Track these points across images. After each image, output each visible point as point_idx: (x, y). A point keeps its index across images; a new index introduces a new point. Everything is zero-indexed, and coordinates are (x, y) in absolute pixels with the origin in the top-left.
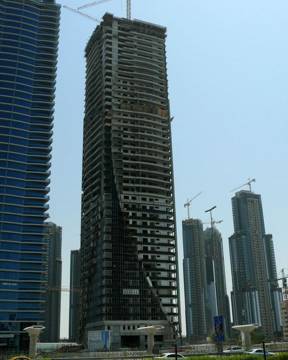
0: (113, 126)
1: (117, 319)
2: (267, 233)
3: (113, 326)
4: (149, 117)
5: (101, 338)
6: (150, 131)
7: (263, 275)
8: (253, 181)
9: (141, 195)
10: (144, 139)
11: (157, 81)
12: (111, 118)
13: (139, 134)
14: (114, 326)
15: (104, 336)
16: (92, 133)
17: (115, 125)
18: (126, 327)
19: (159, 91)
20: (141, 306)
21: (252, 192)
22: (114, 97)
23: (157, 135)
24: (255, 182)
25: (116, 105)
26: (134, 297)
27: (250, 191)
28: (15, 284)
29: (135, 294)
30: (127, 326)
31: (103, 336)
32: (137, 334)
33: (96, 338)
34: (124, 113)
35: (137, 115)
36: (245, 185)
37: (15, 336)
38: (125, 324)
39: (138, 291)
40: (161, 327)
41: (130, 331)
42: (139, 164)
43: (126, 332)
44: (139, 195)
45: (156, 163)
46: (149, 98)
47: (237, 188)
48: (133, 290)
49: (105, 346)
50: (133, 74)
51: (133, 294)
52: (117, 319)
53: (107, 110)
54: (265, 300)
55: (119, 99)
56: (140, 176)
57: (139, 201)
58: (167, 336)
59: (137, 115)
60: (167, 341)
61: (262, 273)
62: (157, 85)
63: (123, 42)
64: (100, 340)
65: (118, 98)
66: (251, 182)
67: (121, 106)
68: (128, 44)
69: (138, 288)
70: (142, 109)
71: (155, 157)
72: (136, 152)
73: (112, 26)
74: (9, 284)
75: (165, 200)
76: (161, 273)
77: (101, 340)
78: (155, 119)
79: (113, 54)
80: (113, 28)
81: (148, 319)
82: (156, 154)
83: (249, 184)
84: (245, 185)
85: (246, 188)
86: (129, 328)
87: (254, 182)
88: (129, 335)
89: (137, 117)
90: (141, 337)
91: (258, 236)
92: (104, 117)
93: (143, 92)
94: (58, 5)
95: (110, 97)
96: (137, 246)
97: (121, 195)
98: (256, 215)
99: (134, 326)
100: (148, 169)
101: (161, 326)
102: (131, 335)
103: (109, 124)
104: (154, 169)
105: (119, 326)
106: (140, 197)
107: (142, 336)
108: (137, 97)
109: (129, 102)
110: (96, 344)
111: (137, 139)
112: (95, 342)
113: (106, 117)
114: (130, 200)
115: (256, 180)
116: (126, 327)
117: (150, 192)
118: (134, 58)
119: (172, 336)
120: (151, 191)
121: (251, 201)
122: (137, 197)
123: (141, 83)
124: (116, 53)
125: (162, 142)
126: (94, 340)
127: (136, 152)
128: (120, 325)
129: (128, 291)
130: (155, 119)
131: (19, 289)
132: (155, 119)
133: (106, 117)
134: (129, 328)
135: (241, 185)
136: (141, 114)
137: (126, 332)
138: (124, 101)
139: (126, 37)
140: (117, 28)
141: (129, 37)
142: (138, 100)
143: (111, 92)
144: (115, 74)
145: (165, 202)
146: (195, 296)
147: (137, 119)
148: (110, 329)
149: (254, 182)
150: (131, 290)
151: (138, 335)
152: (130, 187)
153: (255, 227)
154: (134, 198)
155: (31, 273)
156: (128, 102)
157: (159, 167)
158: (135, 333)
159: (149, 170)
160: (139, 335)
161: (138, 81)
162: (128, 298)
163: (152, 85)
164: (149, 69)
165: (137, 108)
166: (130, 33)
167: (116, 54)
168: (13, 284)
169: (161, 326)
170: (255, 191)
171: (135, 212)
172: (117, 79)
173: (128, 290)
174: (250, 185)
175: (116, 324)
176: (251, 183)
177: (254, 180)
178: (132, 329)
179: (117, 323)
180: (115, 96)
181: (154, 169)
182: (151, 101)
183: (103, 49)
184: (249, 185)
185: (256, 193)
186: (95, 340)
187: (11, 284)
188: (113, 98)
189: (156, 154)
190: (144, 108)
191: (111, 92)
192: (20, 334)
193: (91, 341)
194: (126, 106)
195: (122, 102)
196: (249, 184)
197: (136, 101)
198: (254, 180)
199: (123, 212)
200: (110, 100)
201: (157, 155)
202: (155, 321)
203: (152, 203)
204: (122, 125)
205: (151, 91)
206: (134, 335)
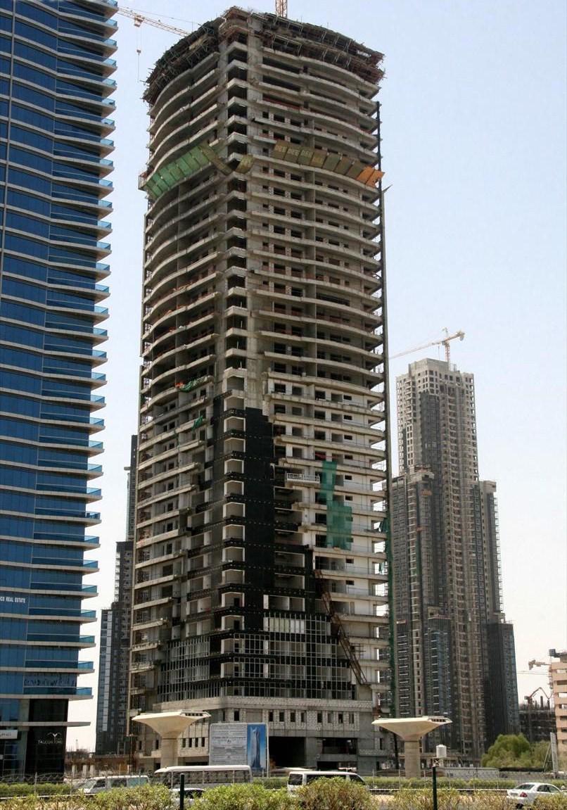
0: (251, 200)
1: (259, 693)
2: (484, 475)
3: (247, 712)
5: (245, 742)
6: (336, 221)
7: (466, 588)
8: (459, 338)
9: (317, 385)
10: (322, 241)
11: (354, 86)
12: (248, 178)
13: (313, 227)
14: (248, 711)
15: (254, 738)
17: (256, 197)
18: (276, 715)
19: (357, 112)
20: (308, 663)
22: (253, 120)
23: (351, 232)
24: (465, 338)
25: (259, 143)
26: (293, 640)
28: (23, 600)
29: (297, 632)
30: (278, 712)
31: (251, 738)
32: (300, 734)
33: (234, 742)
34: (277, 168)
35: (307, 176)
36: (433, 344)
37: (19, 734)
38: (273, 708)
39: (303, 623)
40: (444, 721)
42: (313, 304)
43: (297, 728)
44: (308, 384)
45: (347, 304)
46: (333, 130)
48: (292, 622)
50: (300, 61)
51: (292, 631)
52: (259, 693)
53: (233, 156)
54: (467, 654)
55: (265, 129)
56: (313, 337)
57: (307, 398)
59: (307, 176)
60: (367, 753)
61: (464, 582)
62: (355, 97)
64: (243, 747)
65: (262, 124)
69: (303, 618)
70: (321, 162)
71: (347, 289)
72: (304, 272)
74: (9, 599)
76: (355, 583)
77: (246, 748)
81: (324, 697)
82: (347, 280)
84: (433, 344)
86: (282, 718)
87: (462, 339)
88: (282, 734)
89: (307, 181)
90: (308, 742)
91: (461, 484)
92: (227, 175)
95: (243, 121)
96: (301, 513)
97: (267, 381)
98: (459, 428)
99: (293, 712)
100: (329, 318)
101: (442, 718)
102: (286, 736)
103: (243, 194)
104: (344, 319)
105: (260, 711)
106: (312, 390)
109: (288, 139)
110: (231, 757)
111: (307, 238)
112: (229, 750)
113: (235, 175)
114: (288, 395)
116: (276, 715)
117: (334, 377)
119: (377, 741)
120: (337, 375)
121: (449, 389)
122: (304, 387)
125: (362, 250)
127: (304, 272)
128: (262, 709)
129: (270, 626)
131: (32, 612)
133: (235, 175)
134: (282, 718)
136: (318, 175)
138: (293, 141)
143: (246, 108)
144: (256, 57)
145: (366, 403)
148: (241, 718)
149: (462, 339)
150: (287, 621)
151: (301, 736)
152: (288, 361)
153: (455, 458)
154: (297, 391)
155: (60, 571)
156: (286, 139)
157: (354, 314)
158: (296, 730)
159: (331, 320)
160: (305, 736)
161: (312, 81)
165: (310, 156)
168: (17, 600)
169: (442, 718)
170: (461, 362)
172: (261, 72)
173: (282, 620)
175: (254, 707)
176: (450, 342)
177: (460, 335)
178: (289, 719)
179: (255, 705)
180: (257, 119)
181: (344, 319)
182: (339, 139)
184: (444, 346)
186: (230, 747)
187: (12, 600)
188: (250, 125)
189: (349, 280)
190: (328, 160)
191: (246, 108)
192: (28, 730)
194: (287, 150)
195: (289, 141)
196: (445, 343)
197: (307, 136)
198: (460, 335)
199: (271, 424)
200: (242, 129)
201: (351, 284)
202: (339, 701)
203: (339, 407)
204: (271, 200)
206: (292, 734)
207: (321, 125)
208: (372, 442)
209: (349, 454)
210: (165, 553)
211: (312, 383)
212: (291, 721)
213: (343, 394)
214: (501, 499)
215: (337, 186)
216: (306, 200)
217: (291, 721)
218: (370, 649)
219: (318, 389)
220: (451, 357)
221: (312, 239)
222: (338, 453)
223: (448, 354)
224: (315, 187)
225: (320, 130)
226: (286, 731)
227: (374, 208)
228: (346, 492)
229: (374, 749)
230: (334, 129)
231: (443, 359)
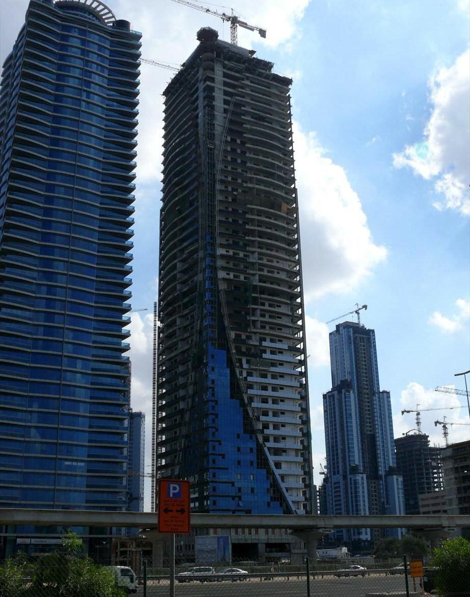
4: (269, 215)
5: (216, 546)
8: (364, 309)
9: (260, 333)
15: (222, 543)
16: (182, 234)
21: (361, 325)
24: (368, 309)
27: (358, 324)
28: (83, 464)
33: (209, 547)
41: (245, 536)
44: (255, 333)
47: (337, 317)
49: (224, 559)
58: (295, 543)
60: (296, 551)
63: (230, 97)
66: (360, 309)
67: (238, 198)
68: (238, 100)
73: (215, 70)
75: (258, 336)
78: (276, 218)
79: (217, 115)
80: (217, 75)
83: (357, 312)
85: (353, 319)
87: (366, 309)
88: (243, 542)
90: (259, 545)
93: (259, 175)
94: (137, 33)
102: (246, 542)
107: (260, 543)
108: (251, 183)
112: (207, 552)
115: (368, 307)
118: (247, 122)
122: (253, 335)
123: (257, 162)
124: (221, 113)
126: (205, 550)
130: (277, 217)
132: (277, 217)
135: (344, 314)
137: (253, 537)
139: (234, 89)
140: (221, 74)
141: (240, 90)
142: (253, 188)
146: (436, 478)
147: (253, 217)
149: (366, 309)
160: (257, 542)
162: (416, 476)
163: (272, 166)
164: (268, 141)
166: (241, 83)
167: (220, 114)
171: (249, 358)
174: (358, 314)
176: (360, 311)
177: (365, 307)
182: (271, 190)
183: (199, 106)
185: (368, 327)
193: (202, 551)
196: (357, 312)
198: (365, 307)
205: (271, 175)
206: (249, 542)
207: (259, 182)
208: (295, 367)
209: (281, 362)
210: (262, 324)
211: (257, 332)
212: (249, 534)
213: (277, 339)
214: (2, 65)
215: (270, 216)
216: (252, 225)
217: (249, 534)
218: (296, 466)
219: (261, 336)
220: (361, 320)
221: (255, 247)
222: (274, 350)
223: (359, 318)
224: (257, 217)
225: (259, 185)
226: (246, 540)
227: (294, 229)
228: (278, 348)
229: (301, 549)
230: (266, 154)
231: (356, 321)
